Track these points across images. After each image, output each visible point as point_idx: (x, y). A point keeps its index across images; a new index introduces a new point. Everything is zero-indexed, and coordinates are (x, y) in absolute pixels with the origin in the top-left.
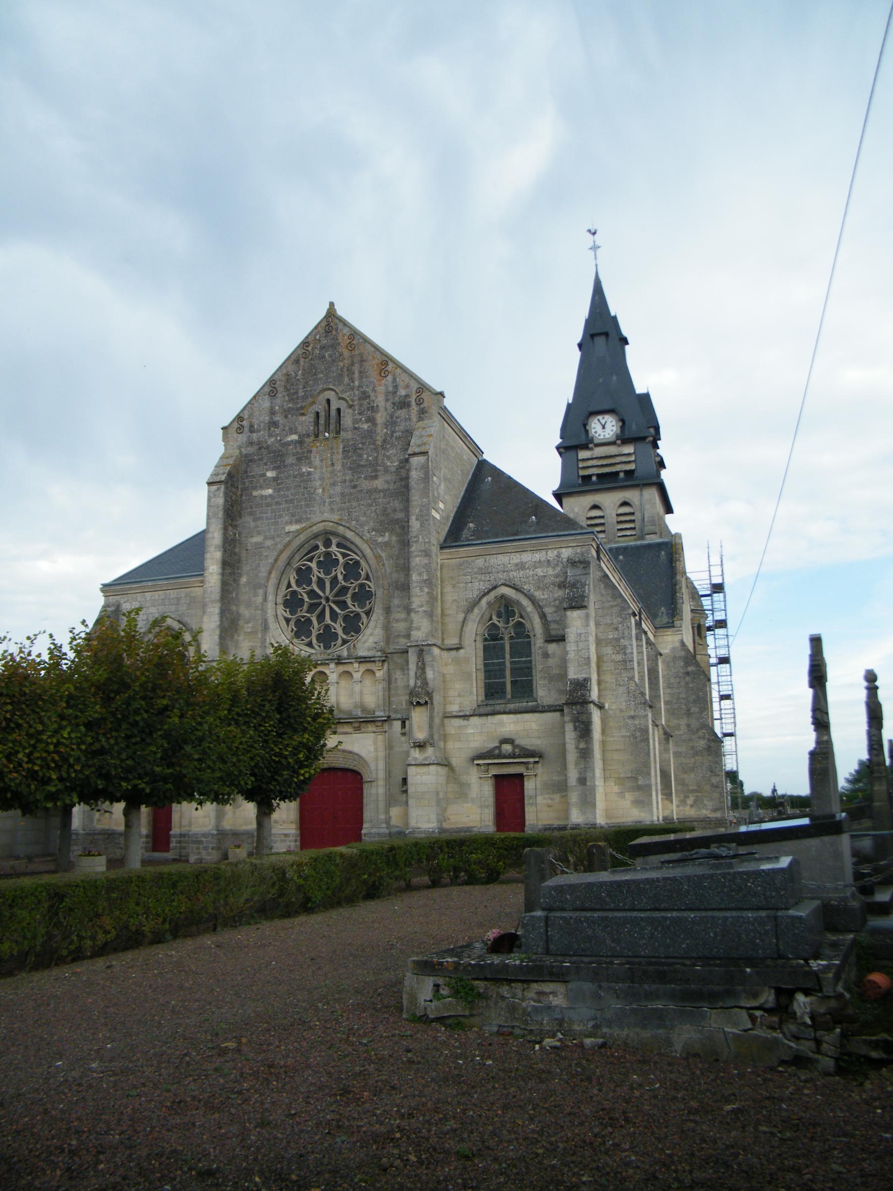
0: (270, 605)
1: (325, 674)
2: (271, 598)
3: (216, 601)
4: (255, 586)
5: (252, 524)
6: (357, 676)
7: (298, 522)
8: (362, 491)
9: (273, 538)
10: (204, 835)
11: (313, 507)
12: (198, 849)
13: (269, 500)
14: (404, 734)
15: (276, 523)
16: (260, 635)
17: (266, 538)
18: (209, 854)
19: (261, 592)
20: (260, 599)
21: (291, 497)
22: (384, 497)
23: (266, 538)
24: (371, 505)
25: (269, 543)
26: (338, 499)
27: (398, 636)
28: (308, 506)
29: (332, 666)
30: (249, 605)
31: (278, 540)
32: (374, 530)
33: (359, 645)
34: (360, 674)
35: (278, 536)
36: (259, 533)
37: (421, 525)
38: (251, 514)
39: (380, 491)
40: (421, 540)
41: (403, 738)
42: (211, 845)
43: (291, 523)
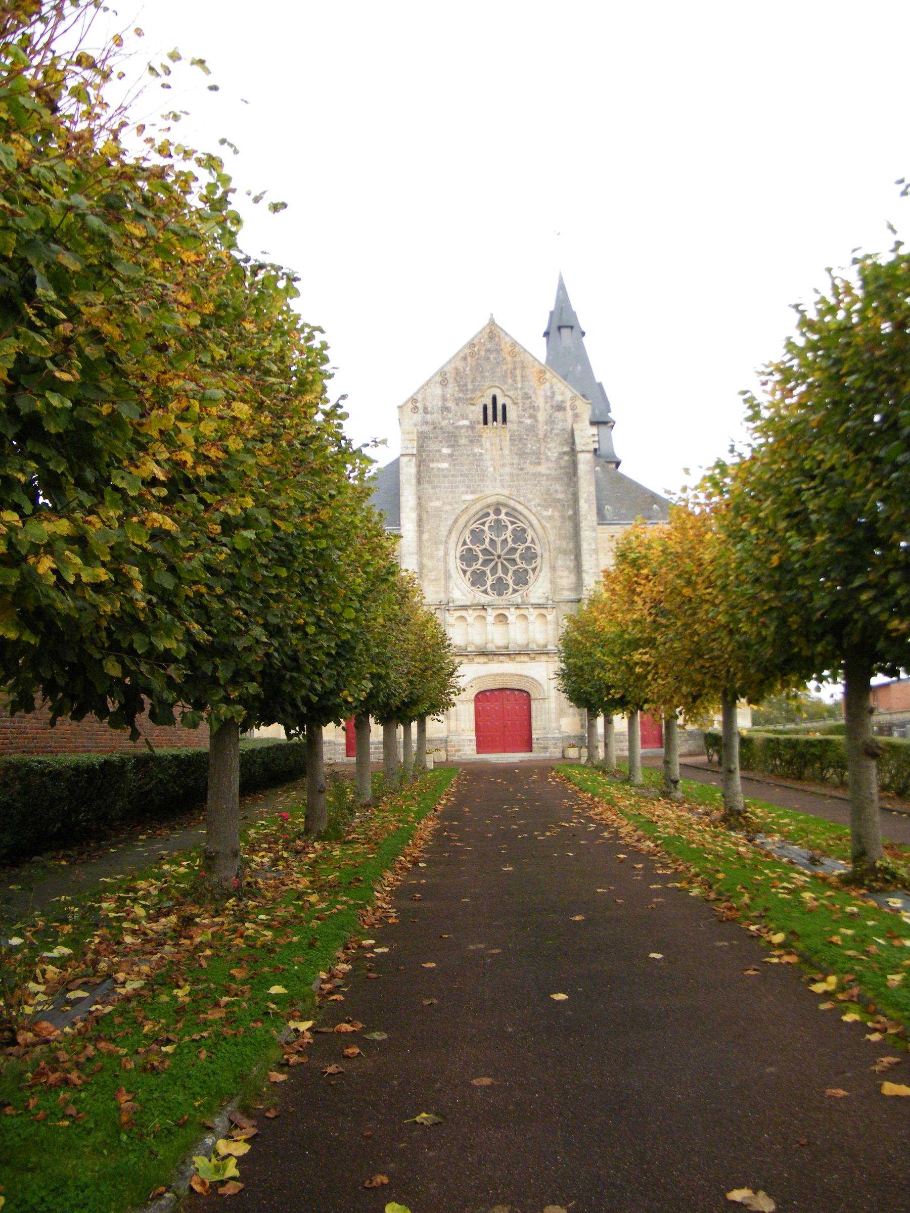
5: (431, 491)
9: (451, 504)
13: (445, 472)
16: (443, 582)
19: (442, 547)
20: (441, 553)
23: (444, 503)
25: (447, 508)
26: (507, 478)
28: (481, 480)
36: (438, 499)
38: (429, 482)
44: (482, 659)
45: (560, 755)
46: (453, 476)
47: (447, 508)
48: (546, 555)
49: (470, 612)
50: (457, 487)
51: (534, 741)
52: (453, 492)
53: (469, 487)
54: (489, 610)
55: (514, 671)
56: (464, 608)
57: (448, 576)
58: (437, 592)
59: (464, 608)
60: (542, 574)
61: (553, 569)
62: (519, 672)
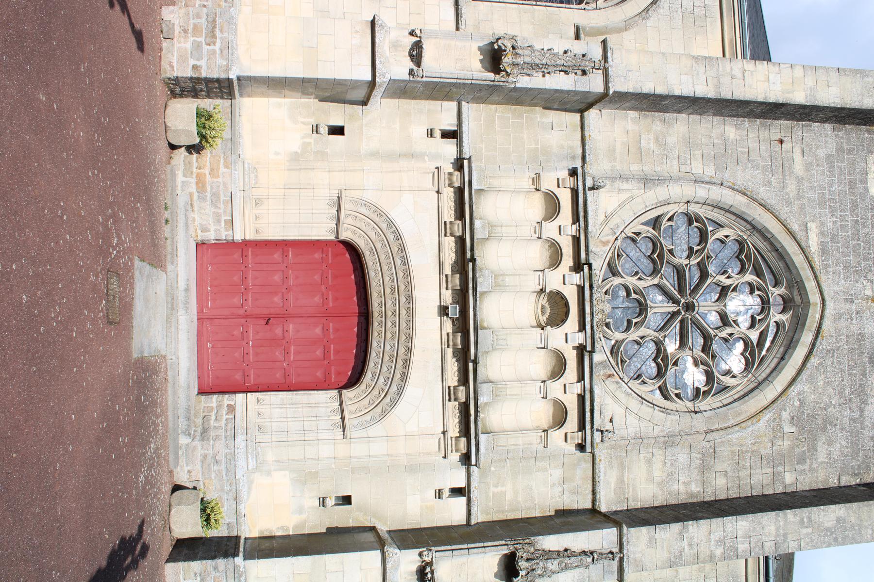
0: (688, 191)
1: (563, 321)
2: (701, 192)
3: (718, 86)
4: (723, 155)
5: (822, 153)
6: (555, 389)
7: (823, 245)
8: (864, 375)
9: (799, 196)
10: (228, 46)
11: (846, 278)
12: (196, 29)
13: (859, 188)
14: (439, 494)
15: (822, 205)
16: (635, 168)
17: (800, 180)
18: (183, 59)
19: (709, 171)
20: (697, 168)
21: (863, 231)
22: (853, 420)
23: (800, 180)
24: (841, 394)
25: (792, 188)
26: (854, 328)
27: (622, 466)
28: (847, 268)
29: (579, 339)
30: (689, 143)
31: (796, 208)
32: (802, 403)
33: (610, 384)
34: (560, 396)
35: (802, 207)
36: (808, 167)
37: (827, 530)
38: (840, 150)
39: (862, 411)
40: (805, 531)
41: (431, 493)
42: (203, 63)
43: (822, 234)
44: (450, 256)
45: (181, 478)
46: (854, 206)
47: (792, 188)
48: (699, 423)
49: (571, 230)
50: (833, 211)
51: (227, 399)
52: (822, 205)
53: (834, 237)
54: (577, 278)
55: (418, 344)
56: (579, 215)
57: (647, 181)
58: (612, 152)
59: (579, 215)
60: (659, 415)
61: (669, 441)
62: (417, 344)
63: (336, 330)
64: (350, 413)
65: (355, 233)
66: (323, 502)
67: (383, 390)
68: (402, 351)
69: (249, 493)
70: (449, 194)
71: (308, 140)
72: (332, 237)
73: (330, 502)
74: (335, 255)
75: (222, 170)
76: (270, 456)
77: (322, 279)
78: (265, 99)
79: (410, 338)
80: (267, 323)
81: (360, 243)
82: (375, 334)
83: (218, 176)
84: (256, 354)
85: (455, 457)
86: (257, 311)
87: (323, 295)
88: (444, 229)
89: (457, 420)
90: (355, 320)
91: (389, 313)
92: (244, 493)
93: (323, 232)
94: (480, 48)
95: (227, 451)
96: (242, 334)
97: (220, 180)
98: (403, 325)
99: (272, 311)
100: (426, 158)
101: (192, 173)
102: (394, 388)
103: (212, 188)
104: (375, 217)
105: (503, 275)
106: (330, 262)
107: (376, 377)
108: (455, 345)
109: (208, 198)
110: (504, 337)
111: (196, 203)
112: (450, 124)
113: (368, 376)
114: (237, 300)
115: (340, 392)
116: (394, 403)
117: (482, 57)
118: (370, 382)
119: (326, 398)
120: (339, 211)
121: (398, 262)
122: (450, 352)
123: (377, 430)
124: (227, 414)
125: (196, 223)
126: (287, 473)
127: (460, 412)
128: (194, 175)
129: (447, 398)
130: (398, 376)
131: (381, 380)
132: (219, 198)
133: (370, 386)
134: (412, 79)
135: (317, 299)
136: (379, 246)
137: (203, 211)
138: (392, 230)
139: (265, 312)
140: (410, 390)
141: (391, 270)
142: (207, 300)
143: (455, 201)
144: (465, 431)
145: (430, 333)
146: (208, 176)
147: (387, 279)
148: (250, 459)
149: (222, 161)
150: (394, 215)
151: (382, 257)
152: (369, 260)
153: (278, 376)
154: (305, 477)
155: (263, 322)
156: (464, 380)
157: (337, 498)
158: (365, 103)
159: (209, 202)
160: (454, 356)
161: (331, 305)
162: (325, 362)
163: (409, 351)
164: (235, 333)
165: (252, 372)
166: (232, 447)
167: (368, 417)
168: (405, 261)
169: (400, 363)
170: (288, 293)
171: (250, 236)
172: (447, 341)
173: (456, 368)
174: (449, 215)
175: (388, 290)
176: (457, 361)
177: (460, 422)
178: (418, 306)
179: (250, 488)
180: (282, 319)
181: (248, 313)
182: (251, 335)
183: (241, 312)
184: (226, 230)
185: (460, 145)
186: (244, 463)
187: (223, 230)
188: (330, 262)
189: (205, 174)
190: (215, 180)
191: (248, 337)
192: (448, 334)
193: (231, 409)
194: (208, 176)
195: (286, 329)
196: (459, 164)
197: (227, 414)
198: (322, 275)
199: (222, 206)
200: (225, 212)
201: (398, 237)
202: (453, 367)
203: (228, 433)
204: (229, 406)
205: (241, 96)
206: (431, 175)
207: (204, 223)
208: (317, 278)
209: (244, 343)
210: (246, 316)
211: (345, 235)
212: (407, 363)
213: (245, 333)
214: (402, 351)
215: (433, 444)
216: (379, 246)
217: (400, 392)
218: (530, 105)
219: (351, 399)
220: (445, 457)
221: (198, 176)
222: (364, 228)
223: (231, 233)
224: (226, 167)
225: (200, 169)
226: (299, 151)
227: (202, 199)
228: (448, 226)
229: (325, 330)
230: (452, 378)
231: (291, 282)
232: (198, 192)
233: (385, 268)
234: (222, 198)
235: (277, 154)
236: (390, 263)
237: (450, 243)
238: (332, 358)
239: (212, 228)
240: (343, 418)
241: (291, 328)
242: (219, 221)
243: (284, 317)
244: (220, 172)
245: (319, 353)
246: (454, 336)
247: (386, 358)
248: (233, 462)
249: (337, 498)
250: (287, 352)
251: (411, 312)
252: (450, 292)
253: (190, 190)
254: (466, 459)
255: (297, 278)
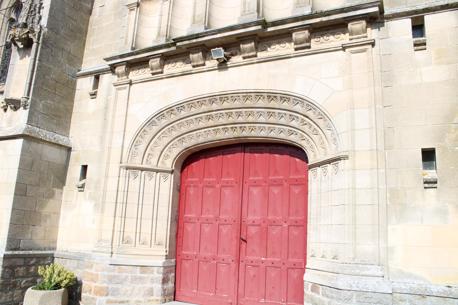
51: (308, 291)
63: (256, 174)
64: (326, 154)
65: (167, 156)
66: (430, 183)
67: (303, 121)
68: (261, 103)
69: (416, 278)
70: (134, 75)
71: (87, 195)
72: (171, 177)
73: (431, 174)
74: (193, 176)
75: (93, 271)
76: (367, 247)
77: (211, 187)
78: (60, 229)
79: (247, 95)
80: (245, 241)
81: (176, 150)
82: (253, 133)
83: (97, 275)
84: (274, 254)
85: (372, 33)
86: (234, 250)
87: (224, 186)
88: (157, 75)
89: (331, 38)
90: (247, 155)
91: (231, 120)
92: (415, 285)
93: (167, 186)
94: (21, 58)
95: (354, 300)
96: (254, 266)
97: (100, 273)
98: (237, 104)
99: (234, 235)
100: (109, 97)
101: (93, 298)
102: (298, 108)
103: (104, 282)
104: (148, 137)
105: (194, 17)
106: (197, 179)
107: (293, 130)
108: (252, 50)
109: (115, 286)
110: (247, 5)
111: (120, 299)
112: (90, 80)
113: (294, 139)
114: (223, 269)
115: (310, 167)
116: (311, 106)
117: (27, 56)
118: (298, 136)
119: (316, 180)
120: (142, 170)
121: (183, 113)
122: (261, 55)
123: (340, 122)
124: (319, 293)
125: (142, 299)
126: (390, 227)
127: (322, 35)
128: (95, 297)
129: (307, 50)
130: (285, 105)
131: (294, 123)
132: (114, 276)
133: (303, 136)
134: (28, 107)
135: (227, 192)
136: (175, 134)
137: (129, 292)
138: (156, 121)
139: (235, 242)
140: (297, 89)
141: (219, 129)
142: (221, 297)
143: (139, 69)
144: (339, 26)
145: (244, 75)
146: (97, 284)
147: (201, 125)
148: (368, 273)
149: (88, 270)
150: (143, 120)
151: (184, 130)
152: (191, 142)
153: (296, 234)
154: (393, 205)
155: (244, 245)
156: (286, 36)
157: (425, 167)
158: (69, 149)
159: (120, 286)
160: (265, 50)
161: (232, 179)
162: (285, 184)
163: (259, 94)
164: (252, 273)
165: (291, 260)
166: (349, 293)
167: (328, 133)
168: (180, 106)
169: (273, 104)
170: (220, 219)
171: (163, 251)
172: (250, 59)
173: (277, 46)
174: (145, 73)
175: (211, 123)
176: (270, 46)
177: (333, 34)
178: (217, 89)
179: (410, 276)
180: (243, 226)
181: (235, 259)
182: (256, 258)
183: (234, 265)
184: (152, 272)
185: (103, 72)
186: (373, 281)
187: (151, 276)
188: (197, 179)
189: (95, 287)
190: (100, 278)
191: (257, 261)
192: (244, 58)
193: (315, 287)
194: (97, 284)
195: (251, 223)
196: (112, 68)
197: (319, 293)
198: (208, 187)
199: (124, 274)
200: (131, 272)
201: (160, 114)
202: (276, 49)
203: (335, 295)
204: (313, 290)
205: (54, 249)
206: (120, 92)
207: (142, 292)
208: (209, 191)
209: (262, 265)
210: (239, 261)
211: (169, 164)
212: (272, 96)
213: (253, 264)
214: (261, 103)
215: (358, 59)
216: (175, 134)
217: (300, 100)
218: (88, 24)
219: (315, 156)
220: (373, 44)
221: (97, 293)
222: (161, 148)
223: (155, 269)
224: (92, 267)
225: (91, 291)
226: (94, 203)
227: (115, 292)
228: (154, 71)
229: (255, 184)
230: (286, 48)
231: (211, 216)
232: (107, 295)
233: (192, 127)
234: (116, 273)
235: (94, 222)
236: (187, 122)
237: (169, 69)
238: (281, 177)
239: (148, 285)
240: (329, 162)
241: (251, 218)
242: (141, 279)
243: (241, 225)
244: (94, 272)
245: (276, 191)
246: (244, 52)
247: (272, 120)
248: (369, 295)
249: (425, 167)
250: (274, 223)
251: (223, 97)
252: (207, 62)
253: (104, 302)
254: (375, 20)
255: (208, 211)
